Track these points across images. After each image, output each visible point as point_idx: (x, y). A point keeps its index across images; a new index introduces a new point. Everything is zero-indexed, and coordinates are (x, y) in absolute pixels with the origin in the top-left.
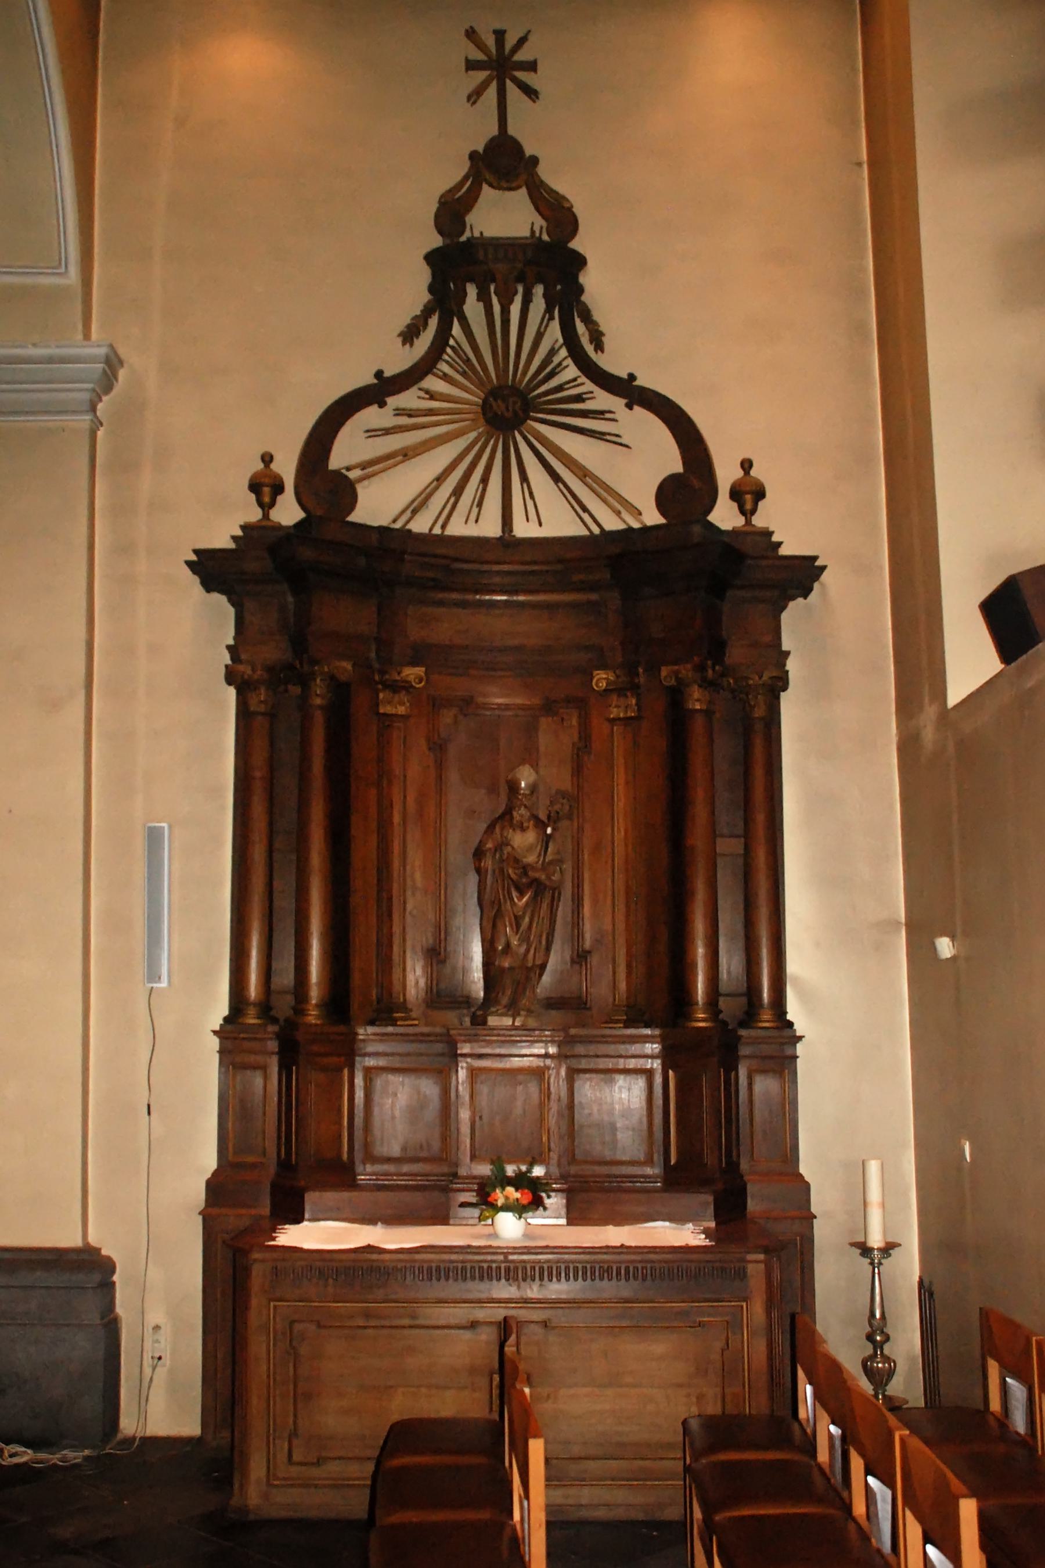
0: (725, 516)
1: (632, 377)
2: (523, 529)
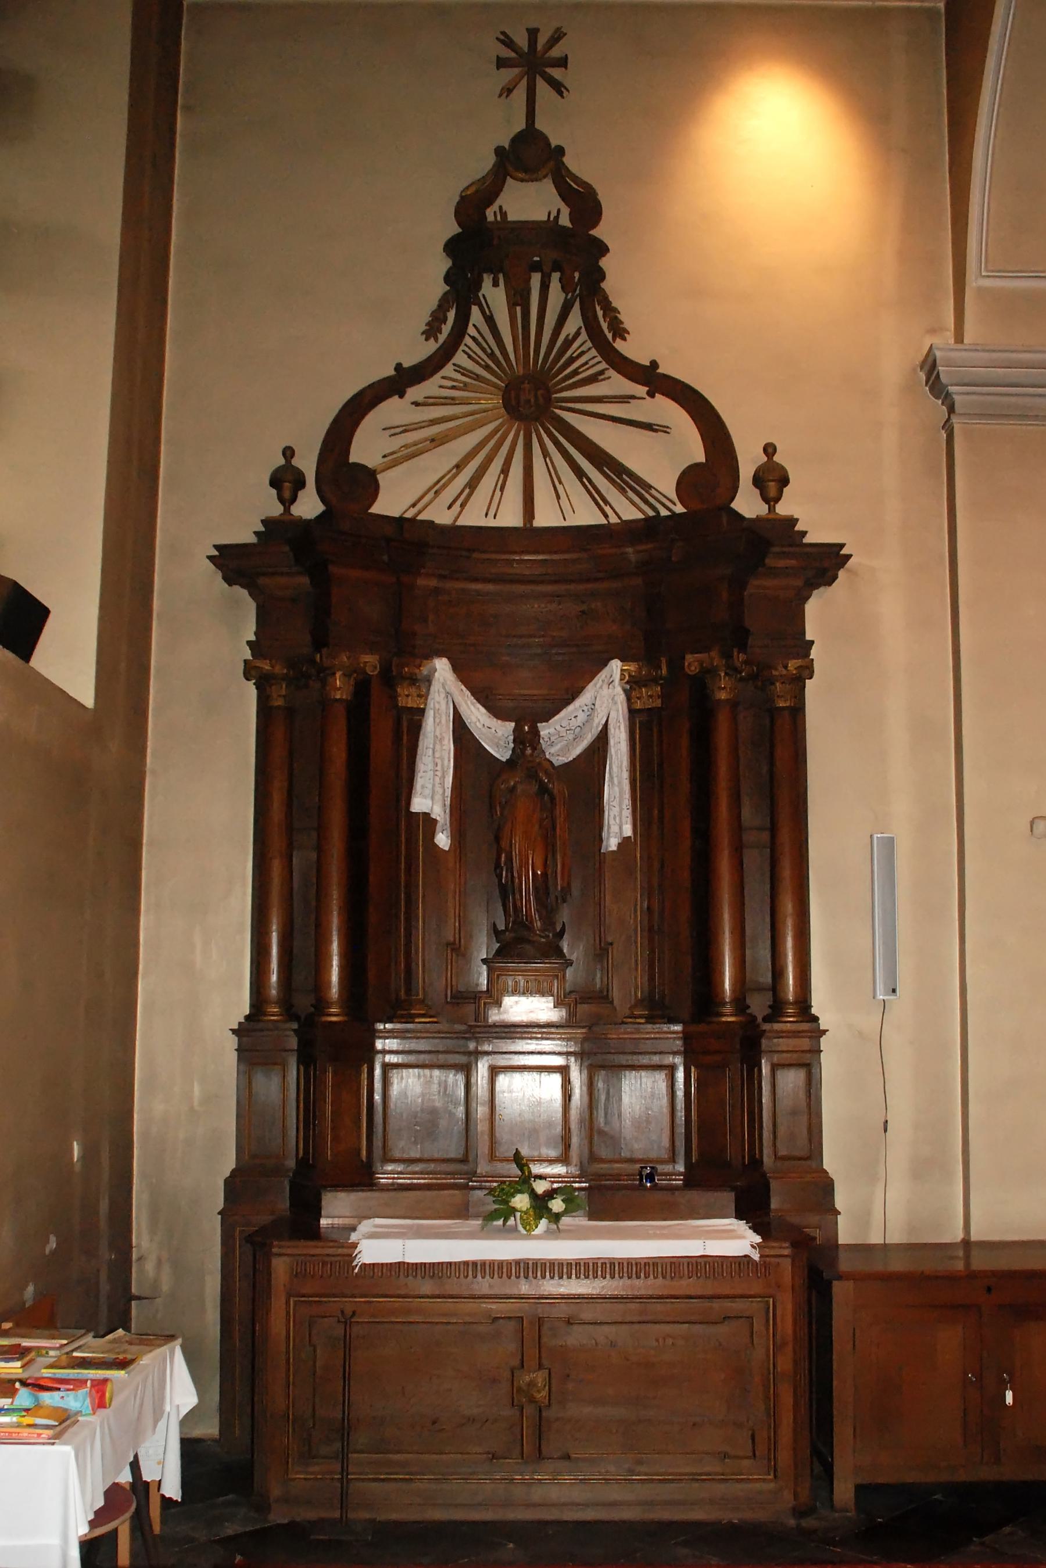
0: (748, 504)
1: (654, 364)
2: (546, 517)
